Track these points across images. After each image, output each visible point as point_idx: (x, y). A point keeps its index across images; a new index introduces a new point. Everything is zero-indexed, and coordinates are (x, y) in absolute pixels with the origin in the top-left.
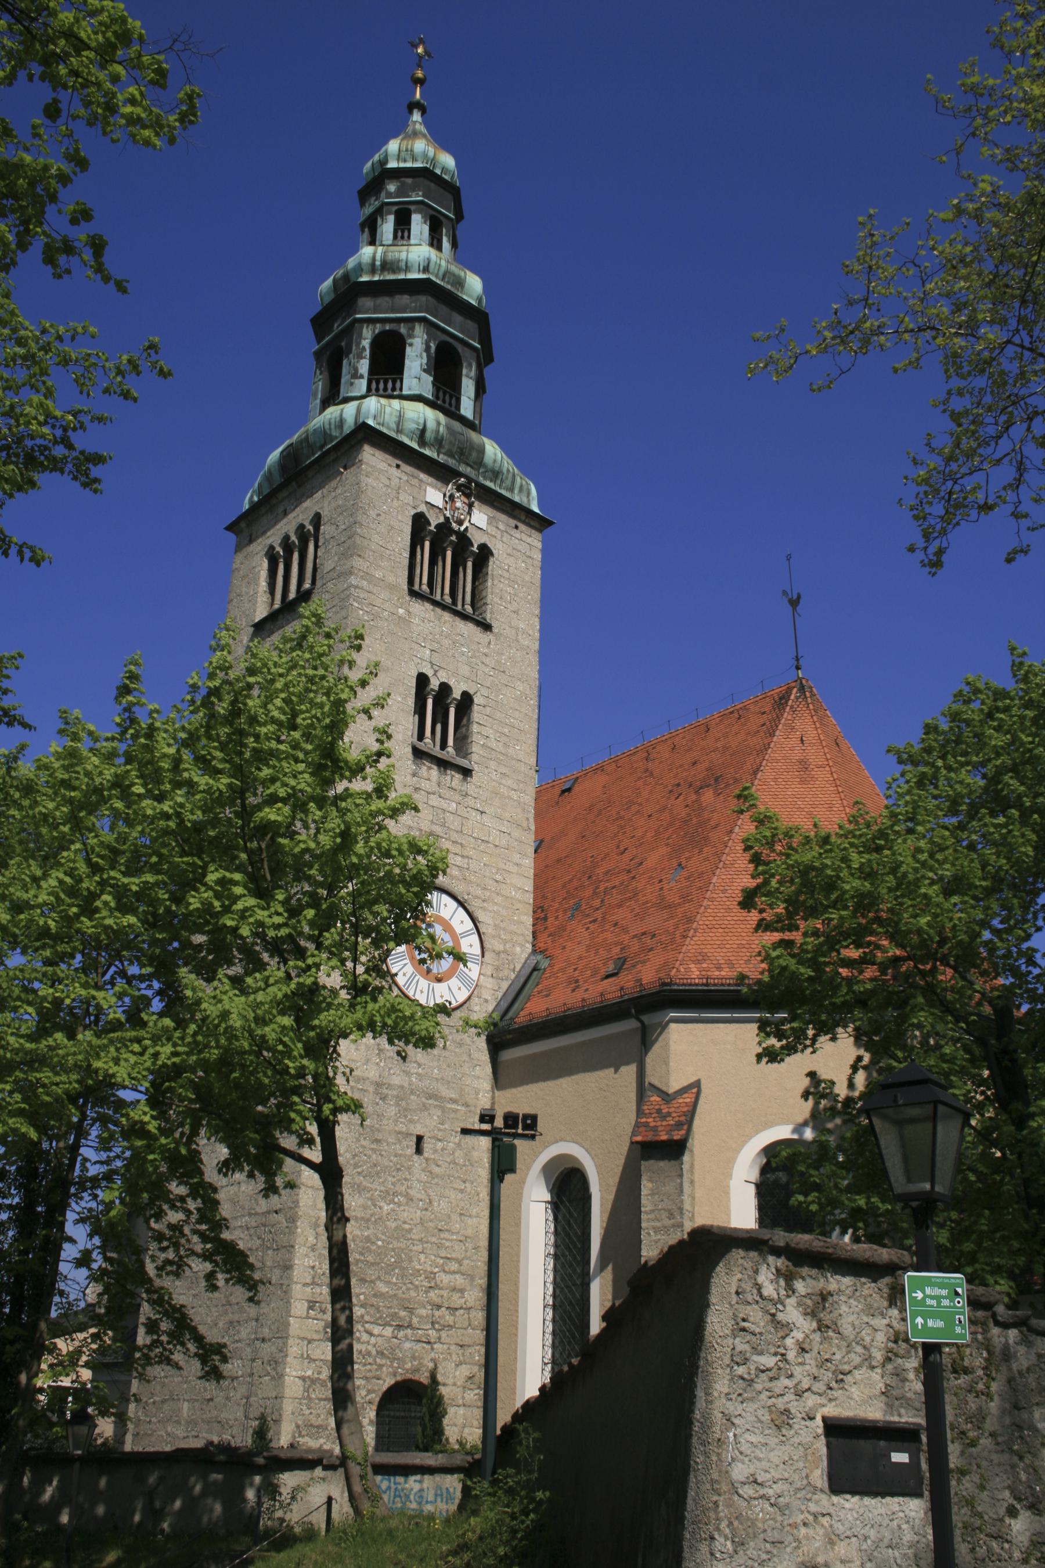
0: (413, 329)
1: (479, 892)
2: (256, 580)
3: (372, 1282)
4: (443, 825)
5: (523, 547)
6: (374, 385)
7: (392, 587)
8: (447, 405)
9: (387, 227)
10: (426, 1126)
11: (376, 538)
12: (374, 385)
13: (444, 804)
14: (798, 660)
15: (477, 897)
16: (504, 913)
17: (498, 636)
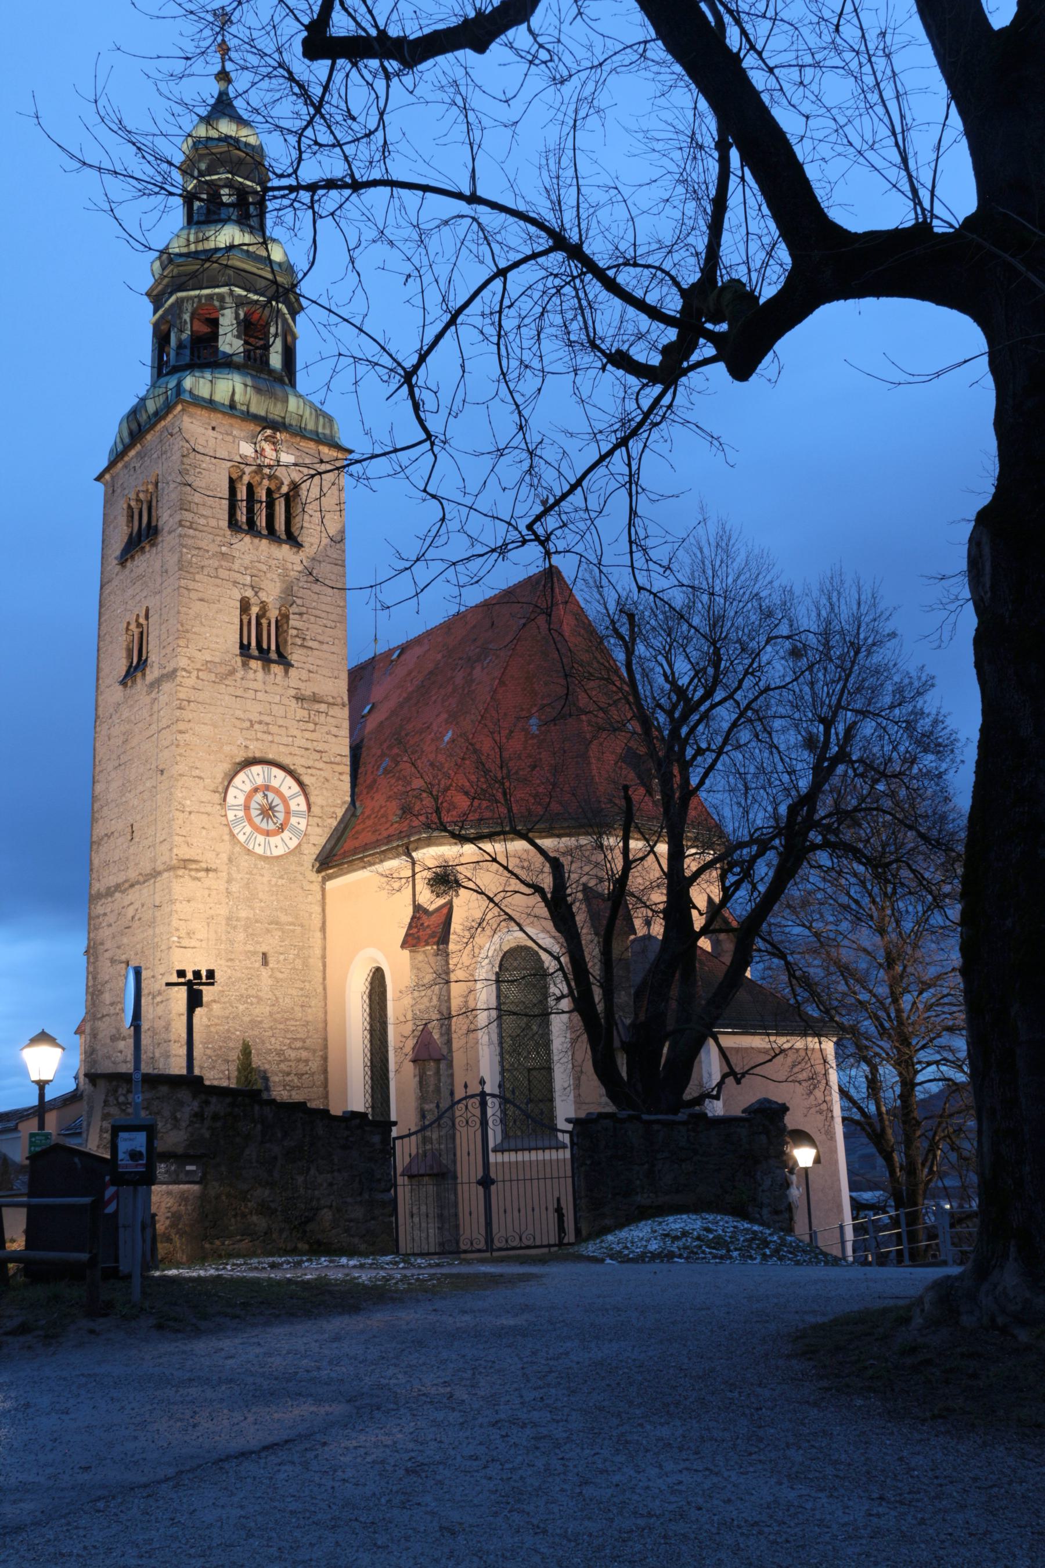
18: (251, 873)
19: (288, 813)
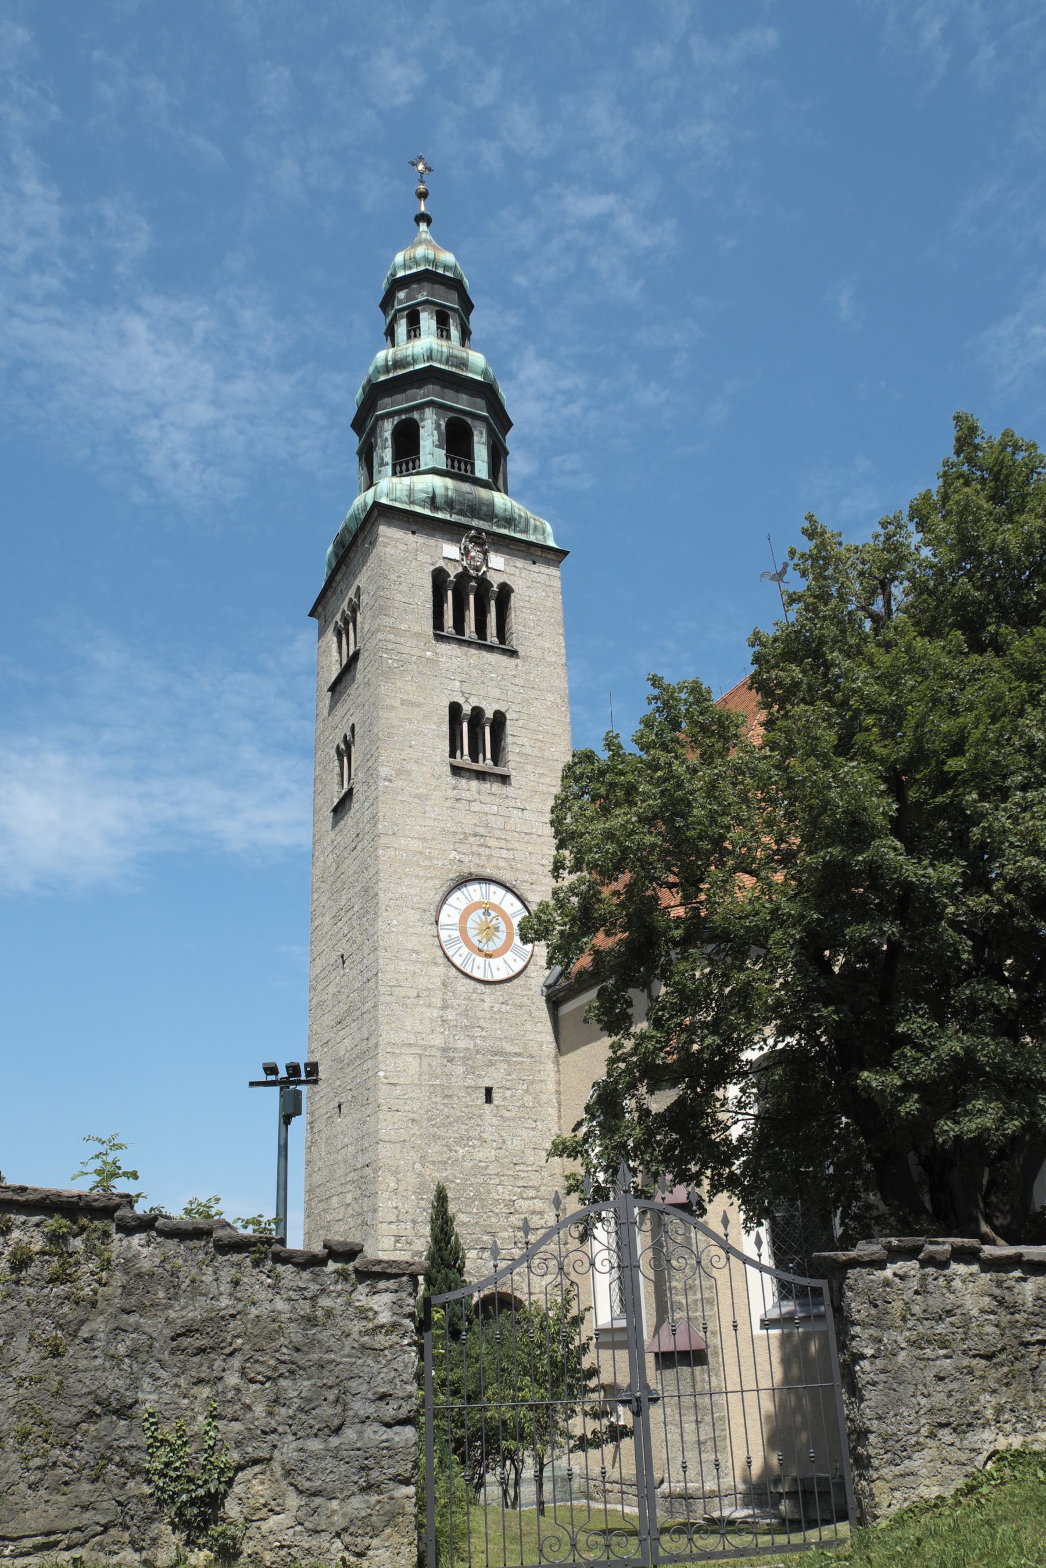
0: (423, 413)
1: (527, 877)
5: (542, 578)
6: (398, 469)
7: (418, 635)
8: (463, 472)
9: (402, 328)
10: (494, 1079)
11: (398, 597)
12: (398, 469)
15: (525, 881)
17: (525, 658)
18: (469, 999)
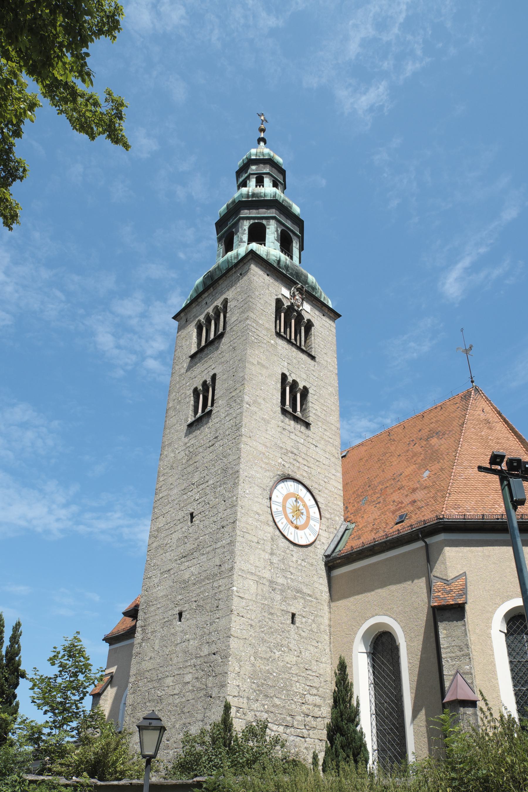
1: (317, 486)
2: (191, 337)
3: (271, 697)
4: (298, 449)
7: (268, 329)
11: (259, 305)
13: (298, 439)
14: (472, 378)
15: (315, 488)
16: (329, 498)
17: (319, 363)
18: (284, 552)
19: (308, 517)
